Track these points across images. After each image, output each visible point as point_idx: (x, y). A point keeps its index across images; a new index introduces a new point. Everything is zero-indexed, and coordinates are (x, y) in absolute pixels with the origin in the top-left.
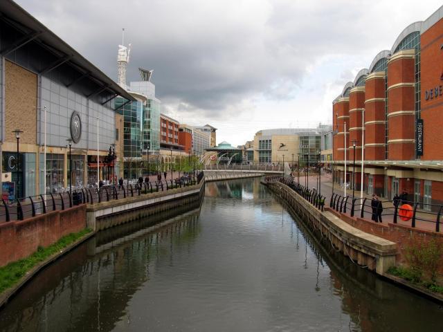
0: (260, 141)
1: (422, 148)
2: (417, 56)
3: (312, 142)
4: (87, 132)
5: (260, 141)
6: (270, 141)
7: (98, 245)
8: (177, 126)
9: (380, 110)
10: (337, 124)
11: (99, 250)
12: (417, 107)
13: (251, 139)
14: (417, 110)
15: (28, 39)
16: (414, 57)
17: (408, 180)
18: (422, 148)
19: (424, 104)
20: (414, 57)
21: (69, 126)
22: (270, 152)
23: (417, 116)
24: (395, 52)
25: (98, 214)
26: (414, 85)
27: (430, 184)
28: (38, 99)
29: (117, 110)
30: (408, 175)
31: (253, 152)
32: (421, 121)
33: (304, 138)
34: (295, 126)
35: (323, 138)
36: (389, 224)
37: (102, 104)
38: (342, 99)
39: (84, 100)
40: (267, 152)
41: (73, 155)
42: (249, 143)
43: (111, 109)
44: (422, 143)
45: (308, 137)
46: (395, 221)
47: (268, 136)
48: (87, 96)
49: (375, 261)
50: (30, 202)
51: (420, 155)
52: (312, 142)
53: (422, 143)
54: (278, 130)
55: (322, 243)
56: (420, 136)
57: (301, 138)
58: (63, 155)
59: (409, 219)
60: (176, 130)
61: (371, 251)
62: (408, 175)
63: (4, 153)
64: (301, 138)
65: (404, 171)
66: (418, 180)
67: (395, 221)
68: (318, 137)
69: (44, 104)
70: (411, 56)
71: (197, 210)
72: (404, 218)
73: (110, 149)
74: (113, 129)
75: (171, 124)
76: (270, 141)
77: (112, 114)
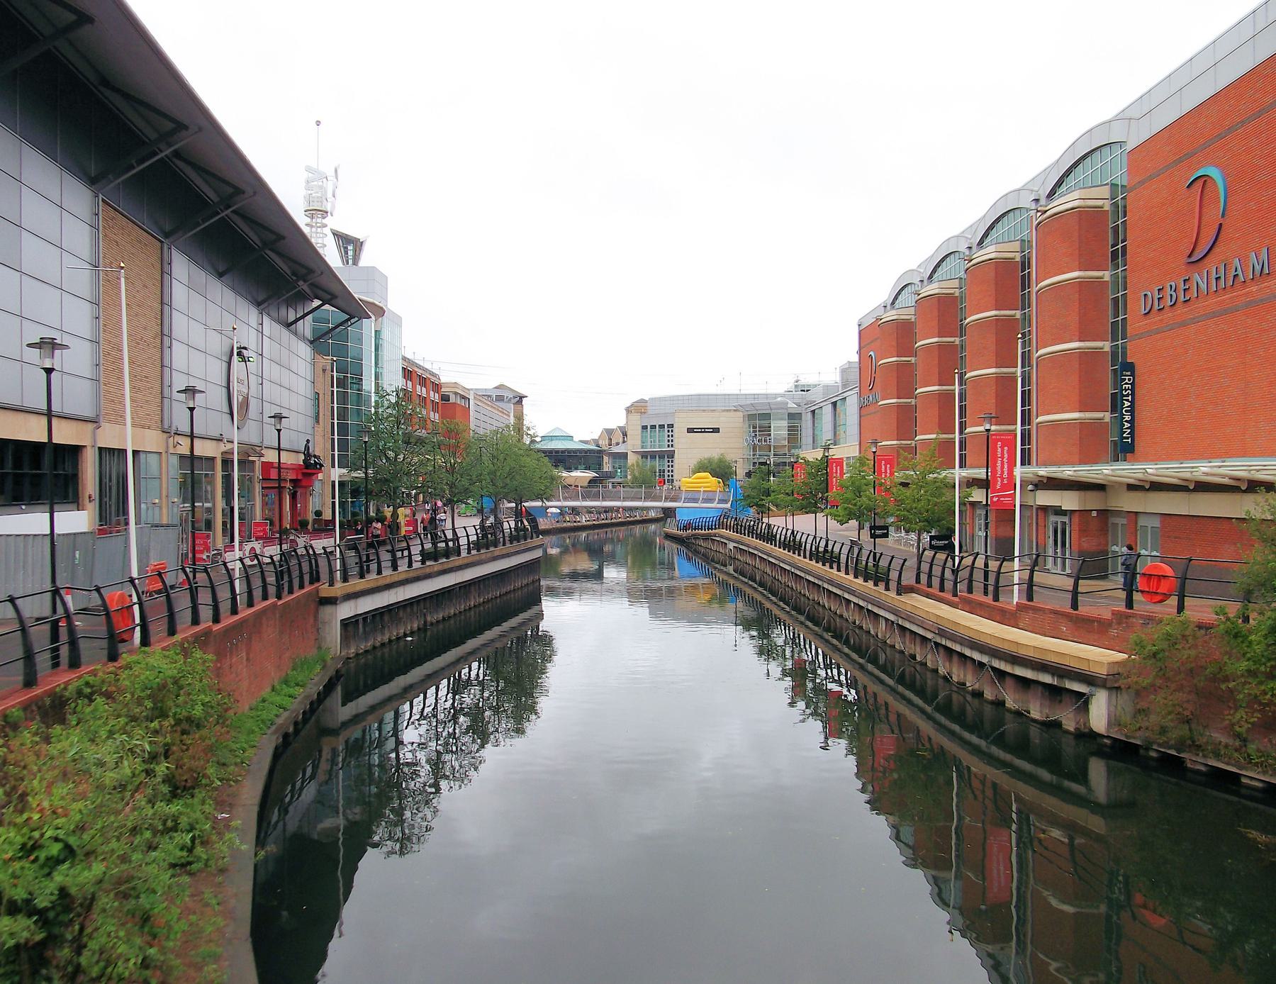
0: (644, 428)
1: (1132, 434)
2: (1115, 205)
3: (779, 429)
4: (1184, 324)
5: (644, 428)
6: (671, 426)
7: (347, 699)
8: (437, 387)
9: (1006, 337)
10: (867, 374)
11: (346, 712)
12: (1118, 331)
13: (618, 419)
14: (1114, 339)
15: (155, 154)
16: (1107, 206)
17: (1094, 514)
18: (1132, 434)
19: (1135, 326)
20: (1107, 206)
21: (224, 384)
22: (671, 455)
23: (1114, 354)
24: (1051, 194)
25: (346, 610)
26: (1106, 275)
27: (1156, 523)
28: (166, 308)
29: (318, 342)
30: (1093, 502)
31: (625, 456)
32: (1130, 367)
33: (758, 420)
34: (731, 388)
35: (828, 409)
36: (1113, 613)
37: (288, 325)
38: (891, 315)
39: (252, 315)
40: (661, 455)
41: (200, 458)
42: (609, 432)
43: (304, 338)
44: (1132, 411)
45: (767, 416)
46: (1130, 603)
47: (666, 415)
48: (258, 304)
49: (1083, 702)
50: (100, 602)
51: (1125, 450)
52: (779, 429)
53: (1132, 422)
54: (690, 398)
55: (901, 680)
56: (1127, 404)
57: (751, 417)
58: (213, 459)
59: (1167, 596)
60: (435, 397)
61: (1063, 685)
62: (1093, 502)
63: (100, 448)
64: (751, 417)
65: (1082, 493)
66: (1118, 513)
67: (1130, 603)
68: (792, 416)
69: (179, 324)
70: (1100, 203)
71: (535, 609)
72: (1153, 595)
73: (307, 448)
74: (310, 394)
75: (423, 381)
76: (671, 426)
77: (305, 350)
